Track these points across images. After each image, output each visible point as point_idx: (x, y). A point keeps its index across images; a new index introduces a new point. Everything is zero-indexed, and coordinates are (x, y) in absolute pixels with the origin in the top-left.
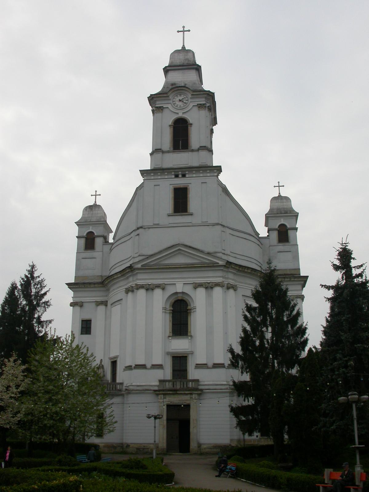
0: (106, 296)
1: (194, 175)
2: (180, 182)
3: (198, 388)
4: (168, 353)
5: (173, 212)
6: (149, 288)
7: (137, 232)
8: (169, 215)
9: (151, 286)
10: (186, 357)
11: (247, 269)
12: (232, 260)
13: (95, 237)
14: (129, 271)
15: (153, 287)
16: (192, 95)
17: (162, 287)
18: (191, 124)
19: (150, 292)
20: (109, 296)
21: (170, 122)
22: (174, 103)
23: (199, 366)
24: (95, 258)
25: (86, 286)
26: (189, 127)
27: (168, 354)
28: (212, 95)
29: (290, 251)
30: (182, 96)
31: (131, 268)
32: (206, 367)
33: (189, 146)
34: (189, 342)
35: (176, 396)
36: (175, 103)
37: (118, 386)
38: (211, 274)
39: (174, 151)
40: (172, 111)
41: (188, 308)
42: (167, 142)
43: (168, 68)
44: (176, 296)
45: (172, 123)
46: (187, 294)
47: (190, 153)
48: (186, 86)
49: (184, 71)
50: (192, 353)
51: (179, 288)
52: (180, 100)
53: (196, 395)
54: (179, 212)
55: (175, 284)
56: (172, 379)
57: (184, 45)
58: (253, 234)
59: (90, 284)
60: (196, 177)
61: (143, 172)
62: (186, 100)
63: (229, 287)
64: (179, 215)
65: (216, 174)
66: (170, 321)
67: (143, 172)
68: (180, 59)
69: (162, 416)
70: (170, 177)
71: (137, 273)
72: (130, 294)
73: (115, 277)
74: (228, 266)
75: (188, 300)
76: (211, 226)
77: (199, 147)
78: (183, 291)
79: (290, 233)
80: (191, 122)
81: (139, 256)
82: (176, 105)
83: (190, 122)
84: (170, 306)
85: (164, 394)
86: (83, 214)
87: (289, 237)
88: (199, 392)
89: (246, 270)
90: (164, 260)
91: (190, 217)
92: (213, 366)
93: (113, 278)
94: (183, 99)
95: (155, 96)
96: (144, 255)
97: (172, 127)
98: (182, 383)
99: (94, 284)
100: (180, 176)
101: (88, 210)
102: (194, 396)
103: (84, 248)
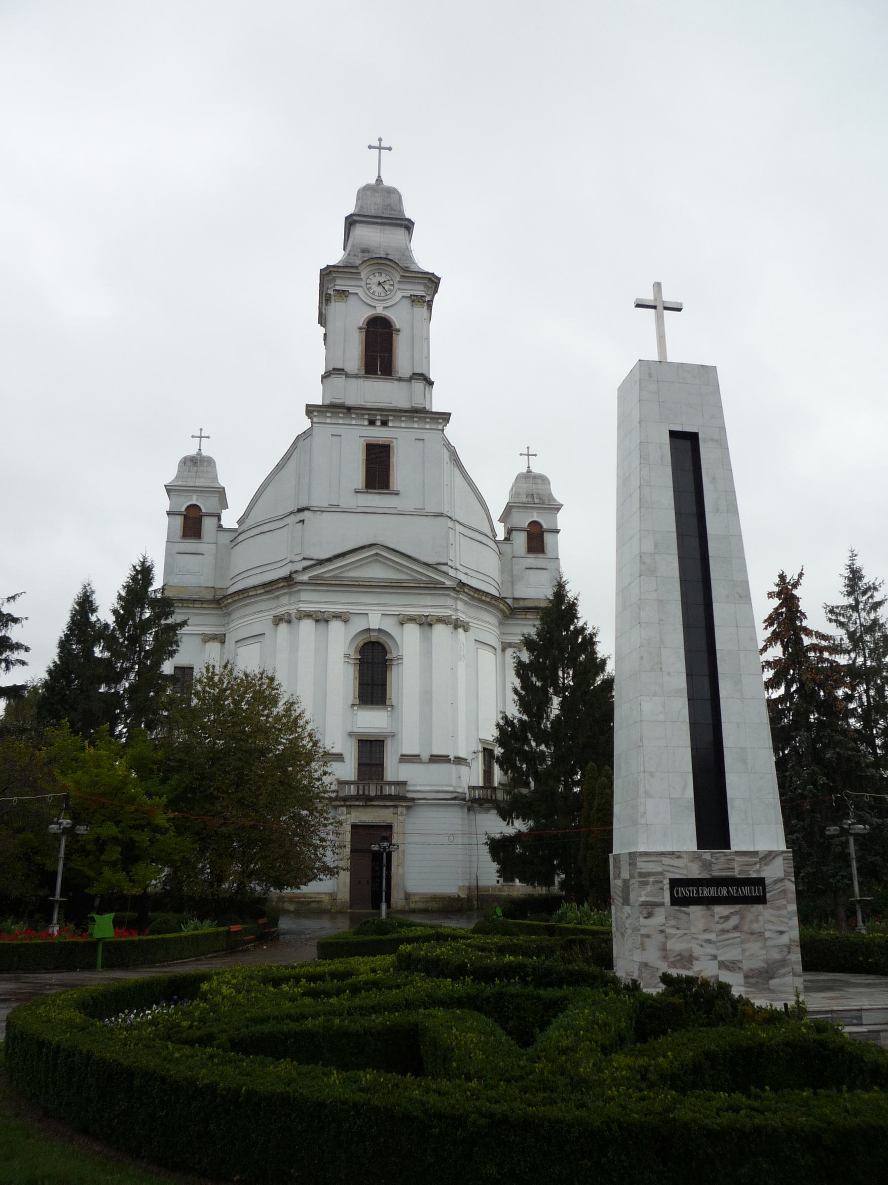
0: (224, 625)
1: (403, 425)
2: (378, 434)
3: (406, 797)
4: (350, 734)
5: (364, 486)
6: (321, 619)
7: (301, 516)
8: (357, 492)
9: (326, 616)
10: (383, 741)
11: (486, 596)
12: (465, 579)
13: (202, 516)
14: (285, 586)
15: (329, 617)
16: (401, 276)
17: (342, 618)
18: (398, 331)
19: (322, 626)
20: (230, 627)
21: (361, 321)
22: (368, 286)
23: (406, 759)
24: (203, 554)
25: (185, 605)
26: (394, 335)
27: (350, 735)
28: (436, 281)
29: (547, 569)
30: (383, 275)
31: (289, 581)
32: (419, 760)
33: (393, 369)
34: (388, 716)
35: (369, 810)
36: (370, 288)
37: (352, 793)
38: (429, 600)
39: (369, 491)
40: (365, 303)
41: (386, 658)
42: (354, 358)
43: (355, 218)
44: (365, 636)
45: (363, 324)
46: (385, 631)
47: (396, 383)
48: (389, 257)
49: (385, 227)
50: (393, 735)
51: (375, 621)
52: (380, 284)
53: (404, 809)
54: (374, 488)
55: (367, 614)
56: (356, 780)
57: (379, 177)
58: (490, 534)
59: (194, 601)
60: (430, 429)
61: (311, 410)
62: (391, 285)
63: (457, 625)
64: (376, 493)
65: (440, 427)
66: (355, 678)
67: (313, 409)
68: (374, 207)
69: (398, 846)
70: (359, 422)
71: (299, 591)
72: (283, 627)
73: (250, 594)
74: (459, 589)
75: (386, 642)
76: (432, 517)
77: (411, 374)
78: (381, 628)
79: (548, 537)
80: (398, 327)
81: (304, 559)
82: (371, 291)
83: (395, 326)
84: (356, 652)
85: (347, 806)
86: (179, 471)
87: (545, 544)
88: (409, 804)
89: (484, 598)
90: (406, 580)
91: (394, 497)
92: (430, 759)
93: (245, 595)
94: (385, 281)
95: (335, 269)
96: (312, 559)
97: (364, 331)
98: (379, 788)
99: (202, 602)
100: (378, 423)
101: (188, 463)
102: (400, 809)
103: (182, 535)
